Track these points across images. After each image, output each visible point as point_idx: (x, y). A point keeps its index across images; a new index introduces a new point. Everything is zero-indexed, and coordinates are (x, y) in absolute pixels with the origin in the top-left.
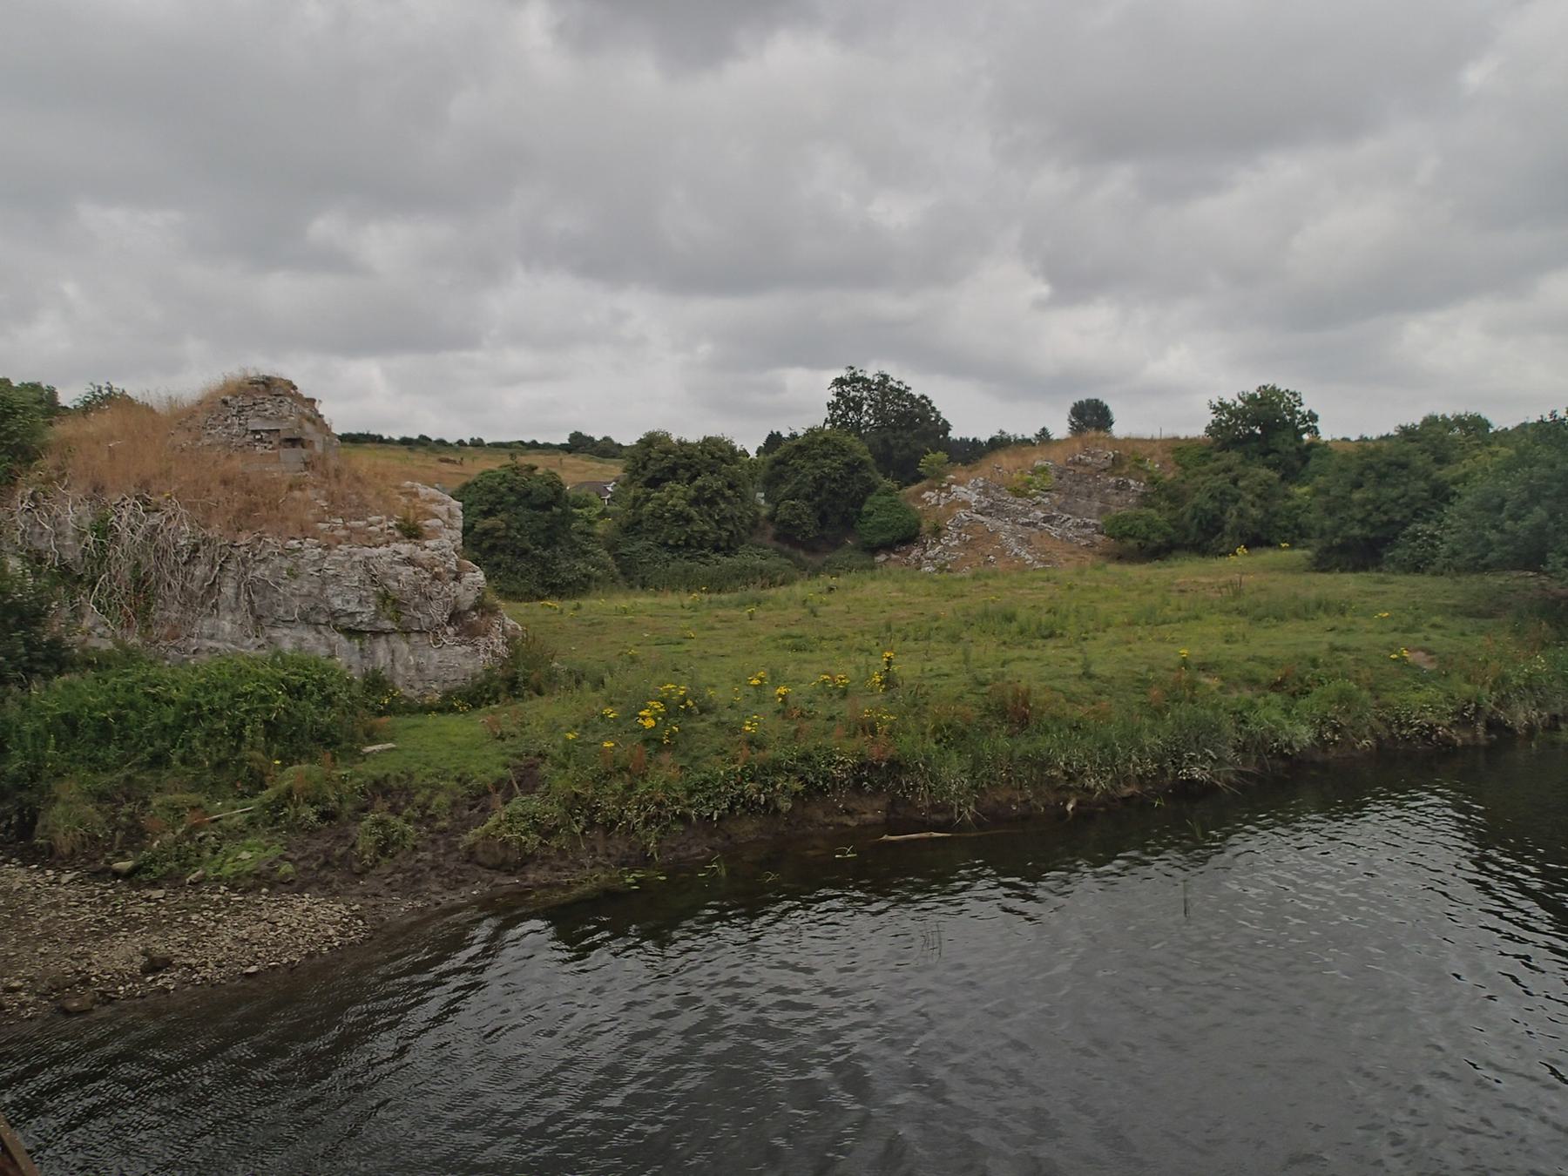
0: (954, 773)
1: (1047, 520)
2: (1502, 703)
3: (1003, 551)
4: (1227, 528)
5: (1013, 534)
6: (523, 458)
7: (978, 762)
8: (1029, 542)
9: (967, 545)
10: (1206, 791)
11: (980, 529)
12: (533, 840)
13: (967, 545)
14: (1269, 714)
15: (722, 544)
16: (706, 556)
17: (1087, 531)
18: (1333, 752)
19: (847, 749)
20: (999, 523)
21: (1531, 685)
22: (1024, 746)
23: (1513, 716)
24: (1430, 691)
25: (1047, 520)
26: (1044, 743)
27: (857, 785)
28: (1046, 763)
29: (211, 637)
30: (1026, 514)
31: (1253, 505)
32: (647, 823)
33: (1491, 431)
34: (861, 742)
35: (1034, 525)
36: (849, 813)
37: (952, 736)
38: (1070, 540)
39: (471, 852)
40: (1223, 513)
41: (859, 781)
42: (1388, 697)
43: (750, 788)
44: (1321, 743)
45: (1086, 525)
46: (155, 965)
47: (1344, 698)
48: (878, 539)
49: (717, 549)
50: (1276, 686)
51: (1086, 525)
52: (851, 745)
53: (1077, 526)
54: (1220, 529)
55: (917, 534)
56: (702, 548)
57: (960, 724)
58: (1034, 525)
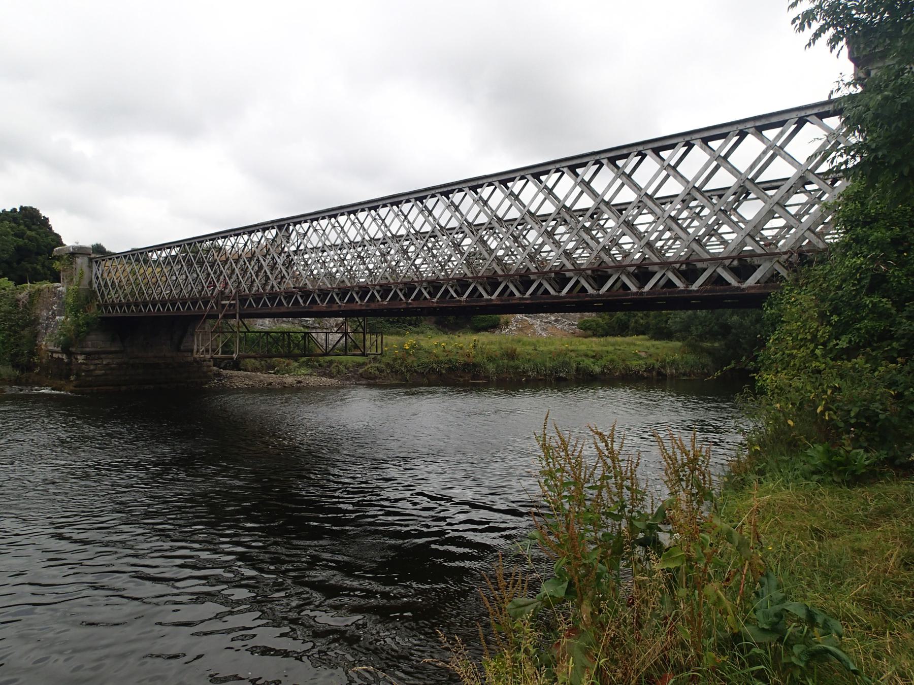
0: (491, 367)
1: (556, 321)
2: (664, 367)
3: (534, 333)
4: (630, 328)
5: (540, 326)
6: (583, 233)
7: (498, 366)
8: (546, 330)
9: (520, 329)
10: (565, 379)
11: (526, 323)
12: (377, 372)
13: (520, 329)
14: (588, 362)
15: (413, 322)
16: (406, 327)
17: (573, 327)
18: (607, 376)
19: (462, 360)
20: (534, 321)
21: (673, 362)
22: (511, 363)
23: (666, 371)
24: (641, 362)
25: (556, 321)
26: (517, 362)
27: (464, 370)
28: (518, 367)
29: (262, 325)
30: (547, 318)
31: (642, 319)
32: (407, 372)
33: (18, 210)
34: (466, 359)
35: (550, 323)
36: (461, 377)
37: (490, 359)
38: (565, 330)
39: (361, 374)
40: (629, 321)
41: (464, 369)
42: (628, 363)
43: (435, 366)
44: (603, 373)
45: (573, 325)
46: (299, 382)
47: (612, 361)
48: (481, 325)
49: (410, 324)
50: (593, 357)
51: (573, 325)
52: (462, 359)
53: (569, 325)
54: (628, 328)
55: (498, 324)
56: (404, 323)
57: (494, 357)
58: (550, 323)
